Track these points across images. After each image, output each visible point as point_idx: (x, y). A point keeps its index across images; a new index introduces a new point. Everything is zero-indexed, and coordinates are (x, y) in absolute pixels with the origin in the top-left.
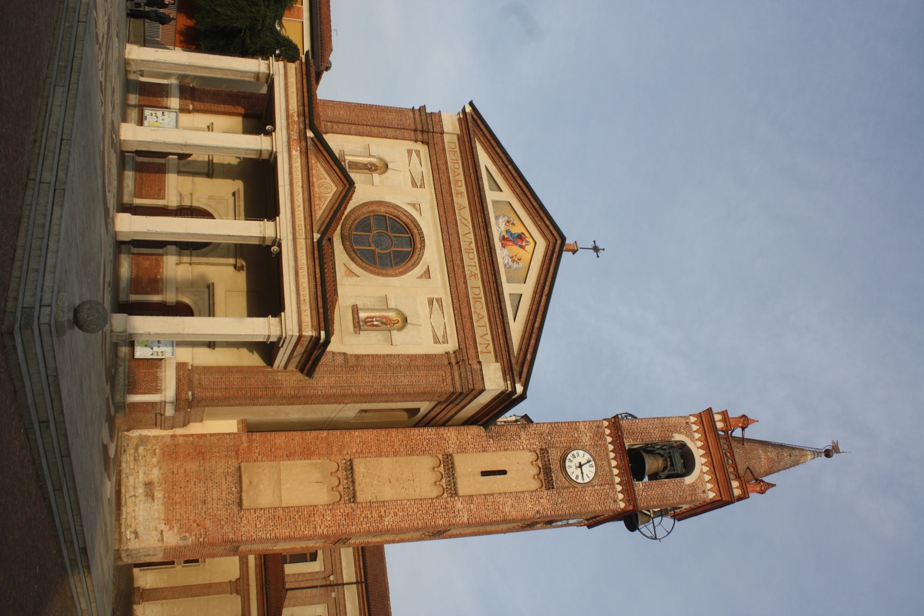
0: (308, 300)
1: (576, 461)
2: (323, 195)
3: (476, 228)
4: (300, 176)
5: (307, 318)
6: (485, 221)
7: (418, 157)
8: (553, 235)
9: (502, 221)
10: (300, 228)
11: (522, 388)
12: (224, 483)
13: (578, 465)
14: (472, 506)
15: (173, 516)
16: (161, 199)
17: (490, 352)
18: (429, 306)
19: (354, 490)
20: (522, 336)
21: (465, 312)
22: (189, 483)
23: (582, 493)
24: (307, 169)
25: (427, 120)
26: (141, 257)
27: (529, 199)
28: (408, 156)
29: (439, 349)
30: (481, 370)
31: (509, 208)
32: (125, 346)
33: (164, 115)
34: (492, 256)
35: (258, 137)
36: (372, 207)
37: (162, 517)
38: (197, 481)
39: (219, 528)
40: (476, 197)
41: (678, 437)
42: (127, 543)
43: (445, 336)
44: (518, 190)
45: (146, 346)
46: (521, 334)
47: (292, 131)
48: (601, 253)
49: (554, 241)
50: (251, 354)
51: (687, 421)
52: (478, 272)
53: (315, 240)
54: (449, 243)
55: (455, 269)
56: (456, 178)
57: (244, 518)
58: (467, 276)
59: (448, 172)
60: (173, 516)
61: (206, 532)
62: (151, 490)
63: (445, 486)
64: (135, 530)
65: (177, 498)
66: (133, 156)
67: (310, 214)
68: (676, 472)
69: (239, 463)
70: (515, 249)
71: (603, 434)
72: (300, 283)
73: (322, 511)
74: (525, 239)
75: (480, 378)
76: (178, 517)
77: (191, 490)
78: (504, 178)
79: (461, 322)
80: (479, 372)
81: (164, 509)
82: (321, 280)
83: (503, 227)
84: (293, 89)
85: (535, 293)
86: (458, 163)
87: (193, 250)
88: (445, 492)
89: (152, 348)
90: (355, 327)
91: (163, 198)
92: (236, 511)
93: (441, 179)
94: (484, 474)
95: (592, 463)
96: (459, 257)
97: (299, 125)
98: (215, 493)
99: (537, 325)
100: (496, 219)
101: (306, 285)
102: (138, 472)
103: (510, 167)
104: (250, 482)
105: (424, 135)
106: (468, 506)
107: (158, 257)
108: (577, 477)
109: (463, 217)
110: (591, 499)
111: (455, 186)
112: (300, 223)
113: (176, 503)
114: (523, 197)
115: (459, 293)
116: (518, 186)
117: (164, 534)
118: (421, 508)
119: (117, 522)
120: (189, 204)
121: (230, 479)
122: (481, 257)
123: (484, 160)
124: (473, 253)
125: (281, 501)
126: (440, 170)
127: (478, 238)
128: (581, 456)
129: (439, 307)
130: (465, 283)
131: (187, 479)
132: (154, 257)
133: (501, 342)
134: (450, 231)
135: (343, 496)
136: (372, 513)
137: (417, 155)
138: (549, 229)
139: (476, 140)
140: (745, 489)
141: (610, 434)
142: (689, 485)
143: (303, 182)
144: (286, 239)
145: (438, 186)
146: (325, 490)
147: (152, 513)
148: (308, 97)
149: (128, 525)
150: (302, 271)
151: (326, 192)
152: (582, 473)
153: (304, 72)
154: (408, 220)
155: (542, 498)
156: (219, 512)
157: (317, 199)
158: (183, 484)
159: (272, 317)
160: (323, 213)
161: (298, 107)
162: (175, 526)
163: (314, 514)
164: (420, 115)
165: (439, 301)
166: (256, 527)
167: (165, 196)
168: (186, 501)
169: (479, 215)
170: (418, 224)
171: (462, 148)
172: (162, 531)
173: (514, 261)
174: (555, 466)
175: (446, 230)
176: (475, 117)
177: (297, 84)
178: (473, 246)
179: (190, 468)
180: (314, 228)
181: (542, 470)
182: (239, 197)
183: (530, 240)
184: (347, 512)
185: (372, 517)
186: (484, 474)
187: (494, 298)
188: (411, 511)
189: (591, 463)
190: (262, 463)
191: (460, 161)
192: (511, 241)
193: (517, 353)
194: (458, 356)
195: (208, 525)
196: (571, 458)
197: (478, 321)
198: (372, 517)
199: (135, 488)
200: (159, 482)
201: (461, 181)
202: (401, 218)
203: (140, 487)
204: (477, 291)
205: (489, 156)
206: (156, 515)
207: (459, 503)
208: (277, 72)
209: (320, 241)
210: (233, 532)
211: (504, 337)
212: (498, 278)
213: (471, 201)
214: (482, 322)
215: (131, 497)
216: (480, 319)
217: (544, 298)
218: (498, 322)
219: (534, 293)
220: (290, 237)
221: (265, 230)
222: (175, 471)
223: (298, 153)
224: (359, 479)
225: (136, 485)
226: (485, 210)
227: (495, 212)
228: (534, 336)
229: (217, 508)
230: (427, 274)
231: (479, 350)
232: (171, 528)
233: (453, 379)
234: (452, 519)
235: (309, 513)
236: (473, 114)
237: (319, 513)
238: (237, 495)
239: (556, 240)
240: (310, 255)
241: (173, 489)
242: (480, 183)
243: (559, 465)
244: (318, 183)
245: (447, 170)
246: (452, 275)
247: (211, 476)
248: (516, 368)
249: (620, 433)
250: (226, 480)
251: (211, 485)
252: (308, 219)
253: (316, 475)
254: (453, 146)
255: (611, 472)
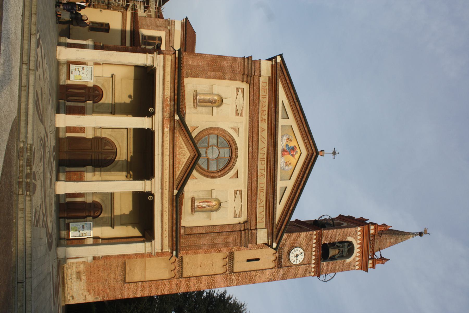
0: (167, 231)
1: (295, 254)
2: (181, 160)
3: (269, 145)
4: (168, 147)
5: (166, 242)
6: (275, 142)
7: (242, 93)
8: (312, 150)
9: (285, 138)
10: (166, 184)
11: (276, 245)
12: (117, 271)
13: (296, 255)
14: (239, 277)
15: (91, 288)
16: (82, 133)
17: (263, 222)
18: (234, 194)
19: (182, 272)
20: (282, 212)
21: (254, 198)
22: (99, 271)
23: (295, 269)
24: (173, 143)
25: (252, 66)
26: (71, 174)
27: (303, 126)
28: (236, 92)
29: (236, 221)
30: (257, 233)
31: (291, 129)
32: (65, 231)
33: (84, 70)
34: (275, 165)
35: (144, 118)
36: (210, 131)
37: (86, 288)
38: (103, 270)
39: (114, 293)
40: (273, 124)
41: (349, 239)
42: (68, 301)
43: (240, 213)
44: (298, 118)
45: (76, 230)
46: (281, 212)
47: (166, 112)
48: (337, 156)
49: (312, 153)
50: (133, 229)
51: (356, 230)
52: (265, 173)
53: (174, 195)
54: (251, 155)
55: (253, 172)
56: (263, 109)
57: (126, 288)
58: (258, 176)
59: (259, 105)
60: (91, 288)
61: (107, 295)
62: (80, 275)
63: (227, 268)
64: (72, 295)
65: (93, 279)
66: (64, 102)
67: (173, 175)
68: (343, 255)
69: (125, 260)
70: (289, 157)
71: (312, 238)
72: (164, 220)
73: (165, 283)
74: (296, 150)
75: (255, 238)
76: (93, 288)
77: (100, 275)
78: (291, 109)
79: (250, 204)
80: (255, 234)
81: (86, 285)
82: (176, 220)
83: (285, 142)
84: (168, 70)
85: (294, 186)
86: (266, 98)
87: (102, 167)
88: (227, 271)
89: (79, 232)
90: (192, 211)
91: (84, 132)
92: (122, 284)
93: (254, 110)
94: (248, 260)
95: (303, 254)
96: (256, 164)
97: (170, 108)
98: (112, 276)
99: (291, 208)
100: (281, 137)
101: (167, 221)
102: (73, 267)
103: (297, 104)
104: (130, 269)
105: (248, 78)
106: (238, 278)
107: (81, 173)
108: (294, 262)
109: (263, 137)
110: (298, 272)
111: (262, 115)
112: (166, 181)
113: (92, 281)
114: (300, 123)
115: (252, 187)
116: (299, 116)
117: (86, 296)
118: (214, 280)
119: (63, 293)
120: (99, 136)
121: (120, 268)
122: (268, 164)
123: (282, 96)
124: (264, 161)
125: (145, 278)
126: (254, 103)
127: (269, 151)
128: (298, 251)
129: (240, 195)
130: (257, 181)
131: (98, 269)
132: (79, 173)
133: (270, 218)
134: (254, 147)
135: (176, 275)
136: (190, 283)
137: (242, 91)
138: (311, 146)
139: (280, 81)
140: (374, 265)
141: (316, 238)
142: (348, 263)
143: (170, 152)
144: (157, 192)
145: (251, 115)
146: (167, 272)
147: (80, 287)
148: (178, 87)
149: (68, 293)
150: (166, 212)
151: (184, 158)
152: (297, 259)
153: (177, 66)
154: (230, 139)
155: (274, 272)
156: (114, 285)
157: (178, 163)
158: (96, 272)
159: (147, 117)
160: (180, 173)
161: (170, 93)
162: (92, 292)
163: (161, 284)
164: (248, 63)
165: (241, 192)
166: (132, 292)
167: (85, 131)
168: (97, 281)
169: (272, 137)
170: (236, 143)
171: (270, 87)
172: (85, 295)
173: (286, 165)
174: (284, 256)
175: (252, 146)
176: (282, 66)
177: (171, 74)
178: (265, 156)
179: (100, 264)
180: (174, 186)
181: (277, 258)
182: (130, 131)
183: (298, 151)
184: (177, 283)
185: (190, 285)
186: (248, 260)
187: (271, 191)
188: (209, 281)
189: (302, 254)
190: (136, 259)
191: (267, 97)
192: (287, 152)
193: (277, 223)
194: (246, 226)
195: (108, 291)
196: (293, 252)
197: (260, 204)
198: (190, 285)
199: (71, 275)
200: (83, 271)
201: (266, 111)
202: (226, 138)
203: (74, 274)
204: (262, 185)
205: (285, 93)
206: (83, 288)
207: (233, 276)
208: (159, 64)
209: (177, 194)
210: (121, 294)
211: (272, 215)
212: (276, 180)
213: (269, 126)
214: (262, 205)
215: (69, 279)
216: (261, 202)
217: (299, 191)
218: (270, 206)
219: (294, 186)
220: (160, 191)
221: (145, 187)
222: (92, 266)
223: (168, 130)
224: (185, 265)
225: (72, 273)
226: (276, 135)
227: (282, 133)
228: (288, 215)
229: (113, 283)
230: (236, 176)
231: (258, 220)
232: (90, 294)
233: (241, 239)
234: (228, 284)
235: (159, 284)
236: (281, 63)
237: (164, 284)
238: (123, 276)
239: (313, 153)
240: (171, 203)
241: (91, 275)
242: (277, 116)
243: (286, 255)
244: (179, 151)
245: (258, 103)
246: (250, 176)
247: (110, 268)
248: (275, 233)
249: (321, 239)
250: (118, 269)
251: (110, 272)
252: (171, 179)
253: (163, 264)
254: (264, 85)
255: (311, 258)
